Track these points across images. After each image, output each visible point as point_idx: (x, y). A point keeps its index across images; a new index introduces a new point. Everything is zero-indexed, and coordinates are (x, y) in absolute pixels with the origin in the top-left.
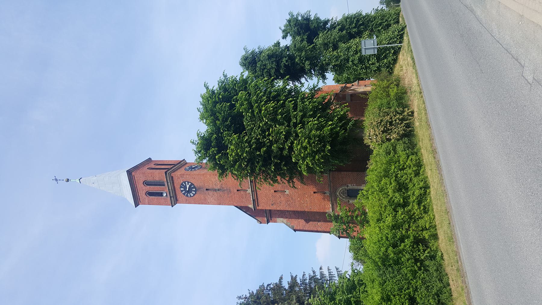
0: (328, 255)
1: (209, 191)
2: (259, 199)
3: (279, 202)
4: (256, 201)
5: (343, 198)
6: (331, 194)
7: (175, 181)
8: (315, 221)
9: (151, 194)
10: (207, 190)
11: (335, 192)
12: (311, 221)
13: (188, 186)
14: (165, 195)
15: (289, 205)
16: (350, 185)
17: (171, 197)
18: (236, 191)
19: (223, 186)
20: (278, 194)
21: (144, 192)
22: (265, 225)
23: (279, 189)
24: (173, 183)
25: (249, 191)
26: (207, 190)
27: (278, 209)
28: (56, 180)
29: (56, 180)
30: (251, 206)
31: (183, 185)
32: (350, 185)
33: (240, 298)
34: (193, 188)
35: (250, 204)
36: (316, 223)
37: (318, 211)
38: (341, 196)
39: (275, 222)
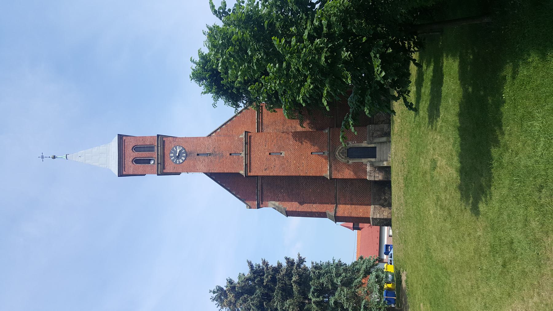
0: (322, 241)
1: (200, 157)
2: (252, 164)
3: (273, 167)
4: (248, 166)
5: (343, 158)
6: (329, 154)
7: (166, 146)
8: (310, 203)
9: (137, 161)
10: (198, 155)
11: (334, 152)
12: (305, 203)
13: (178, 151)
14: (152, 162)
15: (283, 169)
16: (350, 143)
17: (158, 164)
18: (228, 155)
19: (216, 150)
20: (272, 158)
21: (131, 160)
22: (255, 211)
23: (275, 151)
24: (164, 148)
25: (243, 155)
26: (198, 155)
27: (271, 174)
28: (43, 157)
29: (43, 157)
30: (242, 172)
31: (173, 150)
32: (350, 143)
33: (214, 105)
34: (184, 153)
35: (242, 170)
36: (311, 205)
37: (314, 175)
38: (340, 156)
39: (266, 206)
